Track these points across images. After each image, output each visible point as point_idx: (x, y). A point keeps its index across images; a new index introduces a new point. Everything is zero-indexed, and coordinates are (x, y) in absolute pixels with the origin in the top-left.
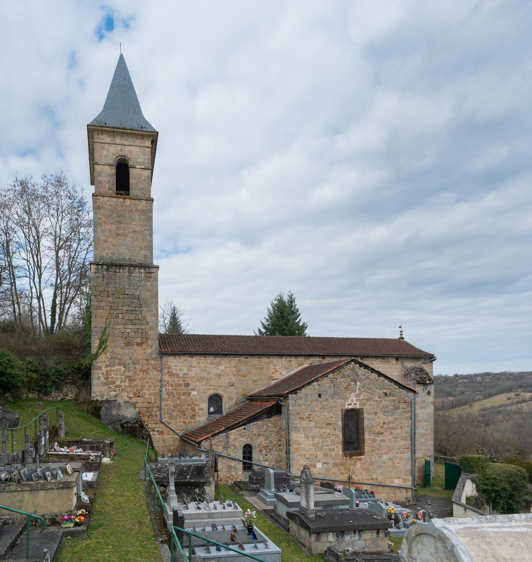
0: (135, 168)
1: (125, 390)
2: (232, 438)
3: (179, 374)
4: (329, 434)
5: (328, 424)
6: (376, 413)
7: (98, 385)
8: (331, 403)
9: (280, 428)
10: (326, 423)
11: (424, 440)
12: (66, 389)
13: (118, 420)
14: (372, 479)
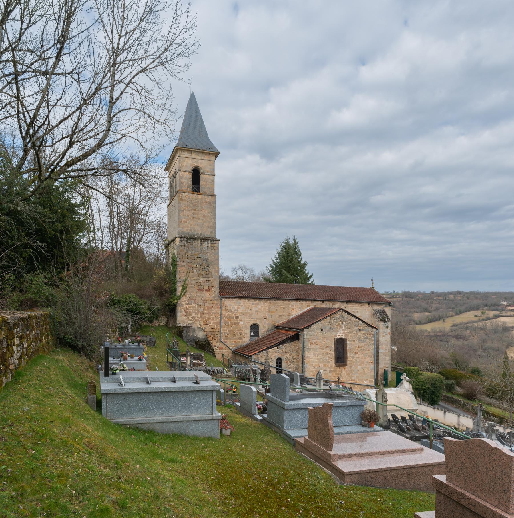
1: (198, 320)
2: (270, 353)
5: (326, 347)
6: (354, 341)
8: (328, 334)
9: (298, 348)
11: (384, 357)
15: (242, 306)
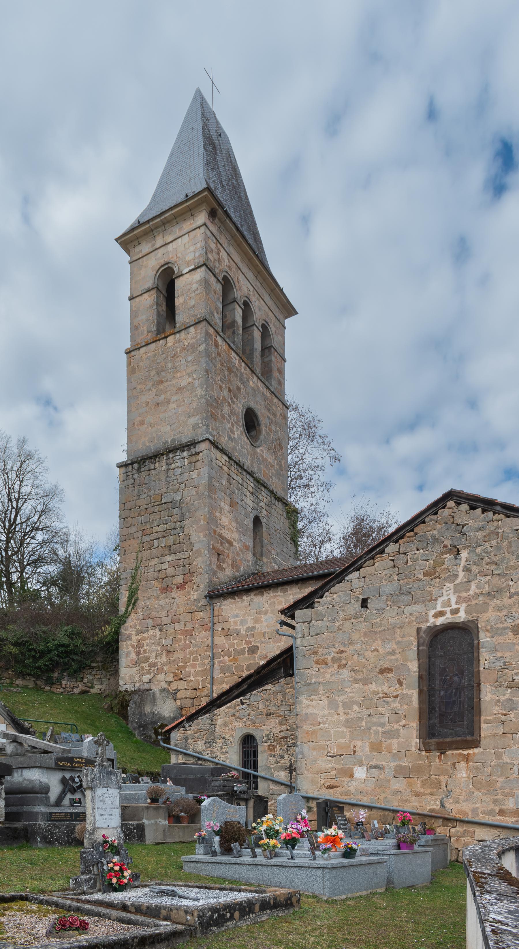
0: (182, 275)
2: (219, 722)
3: (240, 630)
4: (387, 695)
5: (382, 671)
7: (128, 666)
10: (377, 670)
12: (90, 677)
13: (152, 722)
14: (502, 812)
15: (266, 613)
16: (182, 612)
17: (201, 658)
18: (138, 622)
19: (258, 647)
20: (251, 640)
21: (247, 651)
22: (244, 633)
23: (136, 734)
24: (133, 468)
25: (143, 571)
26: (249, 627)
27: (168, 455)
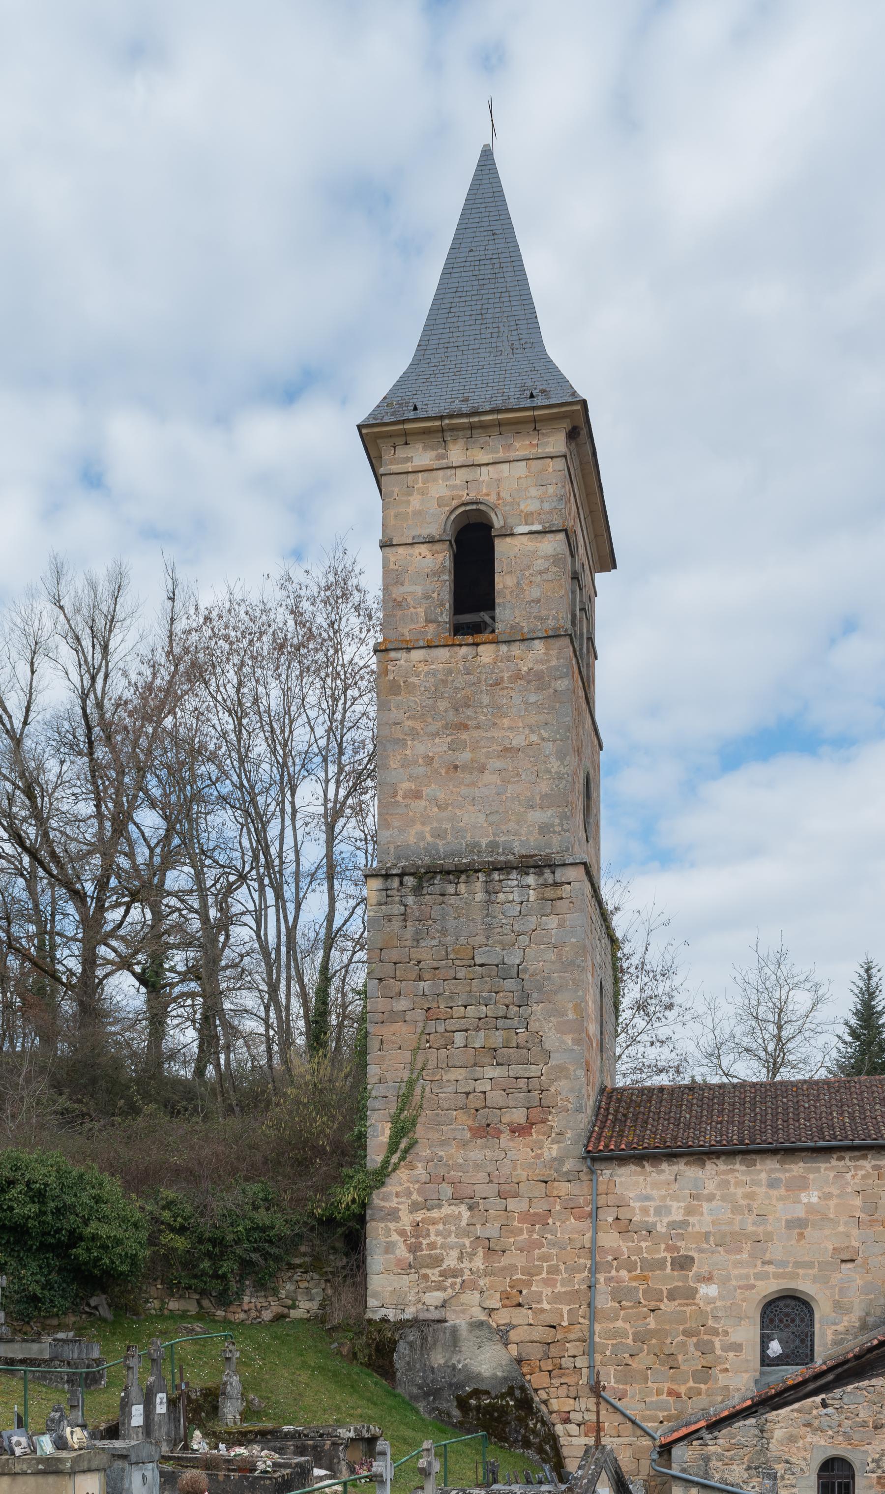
2: (778, 1434)
3: (654, 1224)
12: (289, 1286)
15: (711, 1198)
16: (524, 1178)
17: (566, 1269)
18: (416, 1186)
19: (692, 1259)
20: (679, 1244)
21: (669, 1264)
22: (664, 1230)
23: (421, 1409)
24: (401, 883)
25: (428, 1089)
26: (674, 1222)
27: (489, 875)
